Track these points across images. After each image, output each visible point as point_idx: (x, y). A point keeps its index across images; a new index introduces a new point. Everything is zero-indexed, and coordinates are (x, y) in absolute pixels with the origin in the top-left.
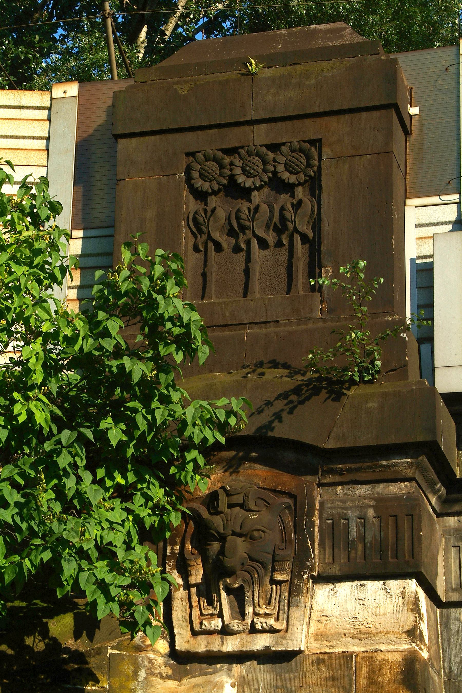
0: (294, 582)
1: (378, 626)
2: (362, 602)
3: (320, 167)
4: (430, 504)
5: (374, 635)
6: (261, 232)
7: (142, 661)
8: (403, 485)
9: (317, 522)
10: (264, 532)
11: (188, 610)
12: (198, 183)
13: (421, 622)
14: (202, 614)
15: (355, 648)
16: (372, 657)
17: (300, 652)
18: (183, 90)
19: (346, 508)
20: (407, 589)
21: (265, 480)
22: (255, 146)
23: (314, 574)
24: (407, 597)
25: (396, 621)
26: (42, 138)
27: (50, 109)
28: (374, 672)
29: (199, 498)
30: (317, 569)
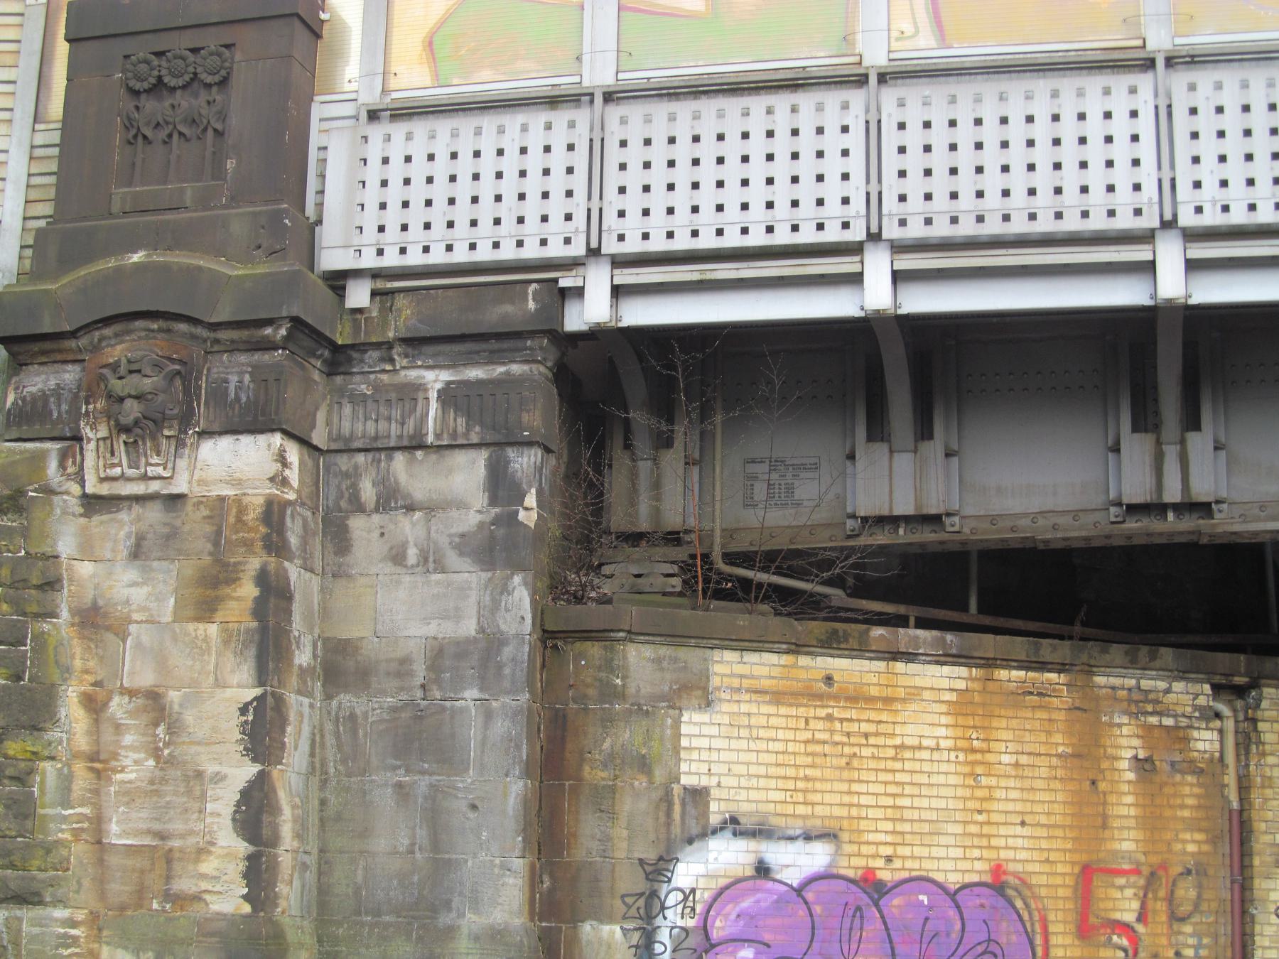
2: (236, 454)
3: (231, 68)
15: (229, 492)
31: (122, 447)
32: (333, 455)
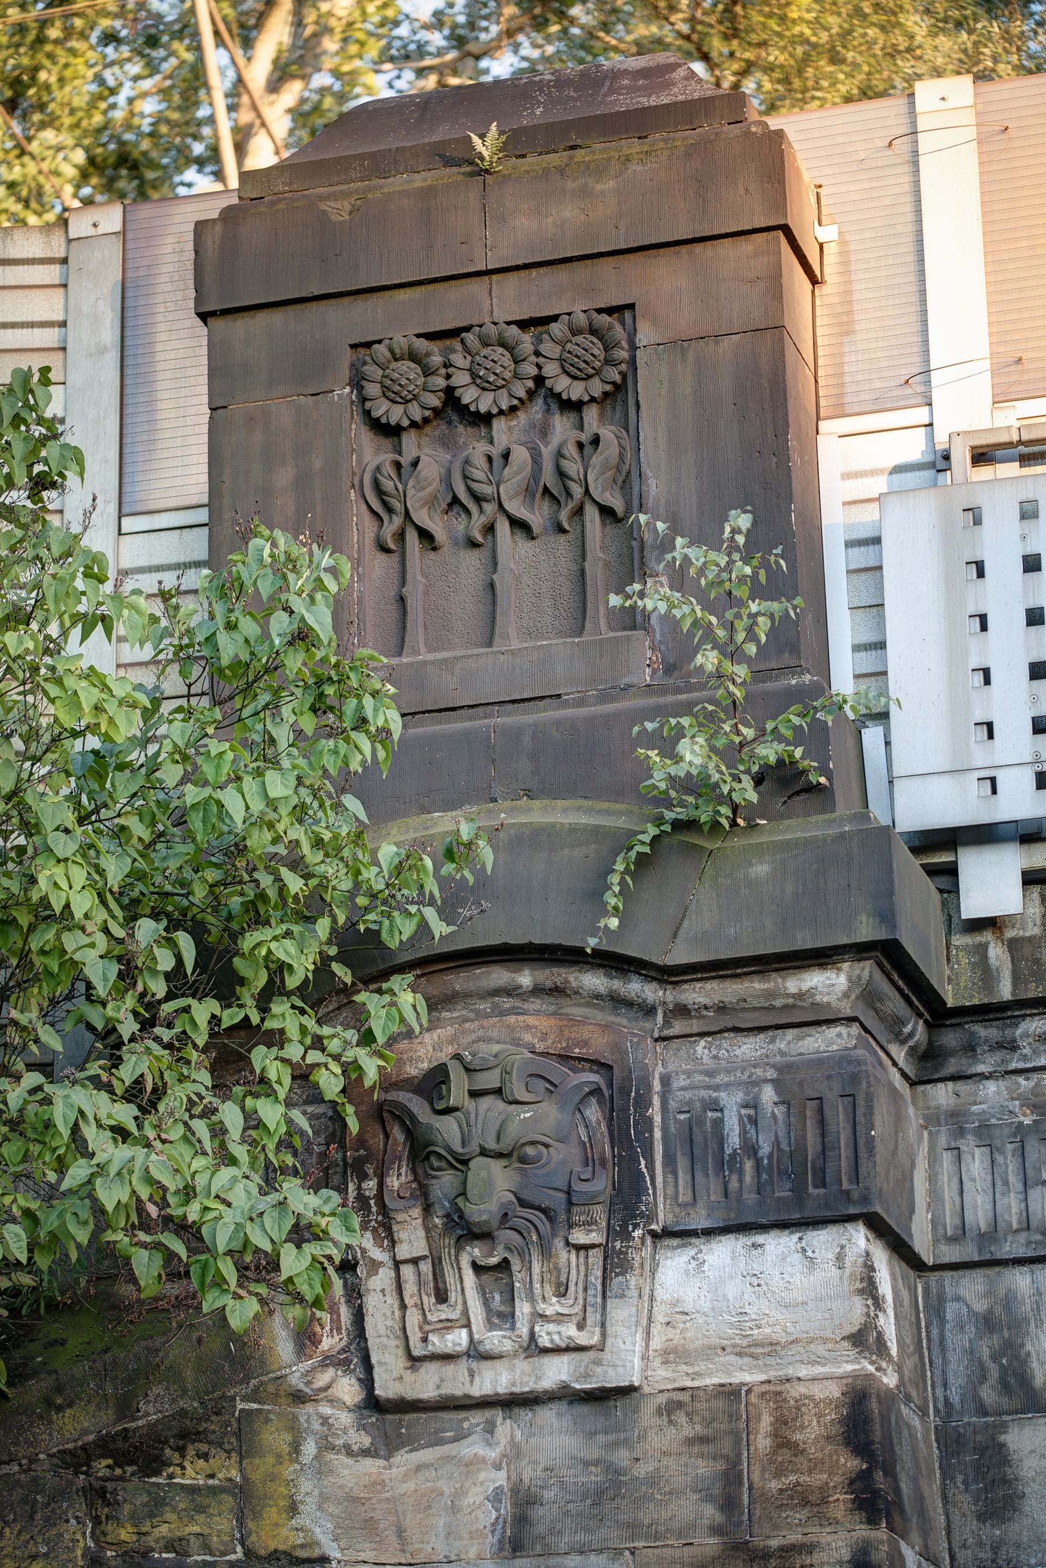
0: (614, 1247)
1: (791, 1328)
2: (756, 1281)
3: (633, 362)
4: (895, 1064)
5: (784, 1347)
6: (516, 508)
7: (308, 1421)
8: (832, 1032)
9: (658, 1119)
10: (547, 1146)
11: (398, 1313)
12: (379, 408)
13: (880, 1314)
14: (426, 1321)
15: (748, 1376)
16: (780, 1393)
17: (629, 1390)
18: (339, 211)
19: (717, 1088)
20: (847, 1249)
21: (544, 1037)
22: (495, 324)
23: (654, 1227)
24: (848, 1264)
25: (827, 1316)
26: (49, 324)
27: (65, 261)
28: (786, 1423)
29: (409, 1081)
30: (661, 1216)
31: (470, 1278)
32: (947, 1275)
